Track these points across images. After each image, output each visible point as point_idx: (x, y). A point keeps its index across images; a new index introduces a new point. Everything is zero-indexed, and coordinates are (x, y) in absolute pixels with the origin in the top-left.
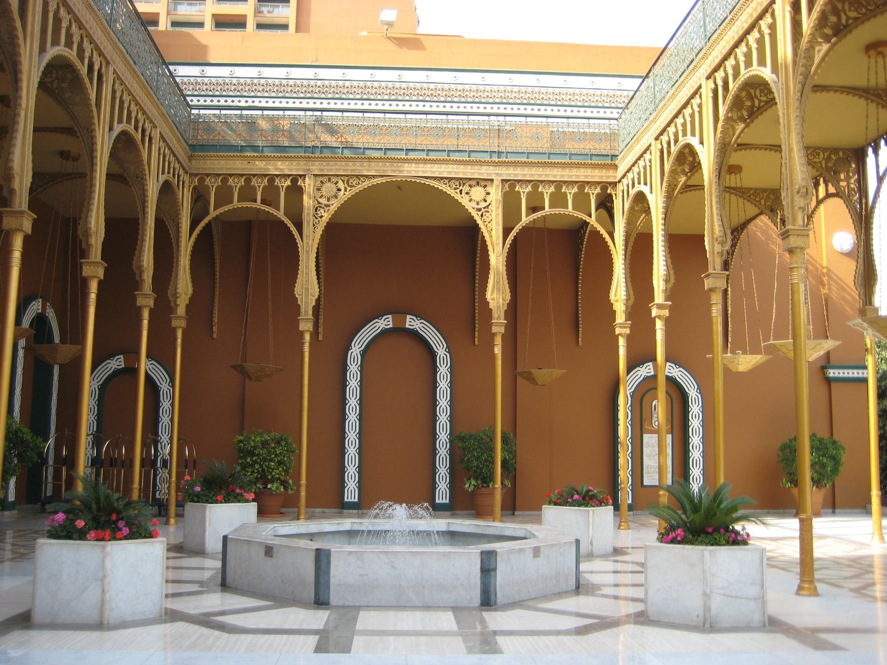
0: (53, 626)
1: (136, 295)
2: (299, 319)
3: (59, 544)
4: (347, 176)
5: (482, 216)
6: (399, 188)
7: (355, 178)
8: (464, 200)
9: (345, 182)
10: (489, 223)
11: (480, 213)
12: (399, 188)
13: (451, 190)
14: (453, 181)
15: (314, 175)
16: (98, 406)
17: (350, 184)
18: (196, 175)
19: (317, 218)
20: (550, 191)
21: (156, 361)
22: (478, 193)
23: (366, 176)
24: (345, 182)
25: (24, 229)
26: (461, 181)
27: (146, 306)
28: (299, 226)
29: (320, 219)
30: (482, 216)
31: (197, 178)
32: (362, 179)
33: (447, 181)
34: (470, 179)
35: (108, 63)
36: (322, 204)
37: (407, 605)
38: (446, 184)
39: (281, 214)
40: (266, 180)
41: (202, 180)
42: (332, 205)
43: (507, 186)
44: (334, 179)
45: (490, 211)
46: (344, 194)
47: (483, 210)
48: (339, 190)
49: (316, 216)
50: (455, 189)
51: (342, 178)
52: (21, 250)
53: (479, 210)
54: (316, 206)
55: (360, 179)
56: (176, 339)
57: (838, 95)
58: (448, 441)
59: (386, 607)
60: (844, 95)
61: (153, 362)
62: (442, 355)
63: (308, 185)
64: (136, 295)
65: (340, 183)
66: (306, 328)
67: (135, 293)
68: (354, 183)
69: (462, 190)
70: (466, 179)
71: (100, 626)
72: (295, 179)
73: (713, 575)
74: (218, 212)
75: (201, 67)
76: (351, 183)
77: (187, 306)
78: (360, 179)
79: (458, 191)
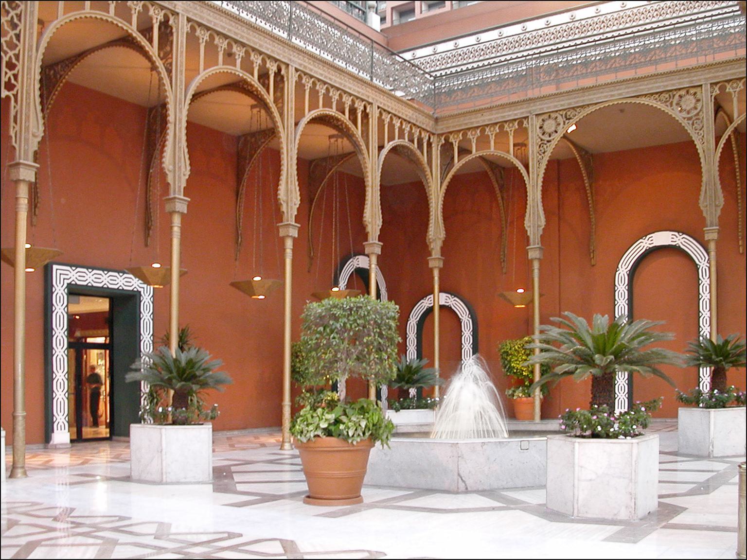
0: (140, 481)
1: (704, 231)
2: (527, 250)
3: (182, 428)
4: (565, 110)
5: (693, 124)
6: (622, 111)
7: (572, 110)
8: (675, 113)
9: (564, 116)
10: (701, 130)
11: (691, 122)
12: (622, 111)
13: (662, 105)
14: (663, 95)
15: (536, 115)
16: (473, 336)
17: (568, 117)
18: (442, 134)
19: (540, 155)
20: (738, 89)
21: (458, 297)
22: (689, 102)
23: (582, 107)
24: (564, 116)
25: (177, 210)
26: (671, 93)
27: (372, 253)
28: (527, 167)
29: (543, 155)
30: (693, 124)
31: (461, 134)
32: (578, 110)
33: (657, 96)
34: (680, 89)
35: (287, 65)
36: (544, 140)
37: (395, 485)
38: (656, 99)
39: (511, 157)
40: (478, 131)
41: (464, 135)
42: (554, 139)
43: (717, 89)
44: (553, 115)
45: (701, 117)
46: (563, 128)
47: (694, 118)
48: (559, 124)
49: (540, 152)
50: (666, 102)
51: (561, 113)
52: (180, 225)
53: (689, 119)
54: (540, 143)
55: (576, 111)
56: (433, 278)
57: (107, 49)
58: (151, 342)
59: (393, 487)
60: (107, 48)
61: (455, 298)
62: (705, 267)
63: (533, 127)
64: (704, 231)
65: (559, 117)
66: (534, 256)
67: (364, 243)
68: (571, 116)
69: (672, 102)
70: (676, 90)
71: (161, 483)
72: (521, 121)
73: (582, 467)
74: (463, 161)
75: (522, 24)
76: (569, 116)
77: (442, 248)
78: (576, 111)
79: (668, 104)
